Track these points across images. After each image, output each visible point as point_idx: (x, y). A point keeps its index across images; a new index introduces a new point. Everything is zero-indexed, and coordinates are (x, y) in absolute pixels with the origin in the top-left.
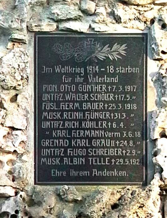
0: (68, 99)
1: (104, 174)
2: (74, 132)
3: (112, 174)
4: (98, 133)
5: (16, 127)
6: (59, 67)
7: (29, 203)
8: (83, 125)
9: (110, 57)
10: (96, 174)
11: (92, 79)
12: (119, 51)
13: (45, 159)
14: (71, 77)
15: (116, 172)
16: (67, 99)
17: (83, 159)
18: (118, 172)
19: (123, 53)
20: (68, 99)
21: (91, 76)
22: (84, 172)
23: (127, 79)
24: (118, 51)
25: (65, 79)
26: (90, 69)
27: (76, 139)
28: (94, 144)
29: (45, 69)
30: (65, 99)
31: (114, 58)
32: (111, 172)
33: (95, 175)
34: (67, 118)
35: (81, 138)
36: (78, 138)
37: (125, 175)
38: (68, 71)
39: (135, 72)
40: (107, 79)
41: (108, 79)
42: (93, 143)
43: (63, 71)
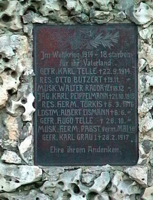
0: (62, 90)
1: (99, 151)
2: (61, 127)
3: (106, 150)
4: (103, 95)
5: (7, 161)
6: (57, 53)
7: (20, 171)
8: (87, 88)
9: (103, 44)
10: (91, 151)
11: (87, 63)
12: (112, 39)
13: (42, 127)
14: (67, 61)
15: (110, 148)
16: (60, 90)
17: (102, 94)
18: (112, 149)
19: (116, 41)
20: (62, 90)
21: (86, 60)
22: (80, 149)
23: (117, 63)
24: (110, 40)
25: (62, 63)
26: (85, 54)
27: (63, 134)
28: (79, 138)
29: (44, 54)
30: (59, 90)
31: (107, 46)
32: (104, 149)
33: (90, 151)
34: (64, 98)
35: (67, 133)
36: (65, 133)
37: (118, 152)
38: (65, 56)
39: (126, 57)
40: (100, 63)
41: (102, 63)
42: (77, 138)
43: (60, 56)
